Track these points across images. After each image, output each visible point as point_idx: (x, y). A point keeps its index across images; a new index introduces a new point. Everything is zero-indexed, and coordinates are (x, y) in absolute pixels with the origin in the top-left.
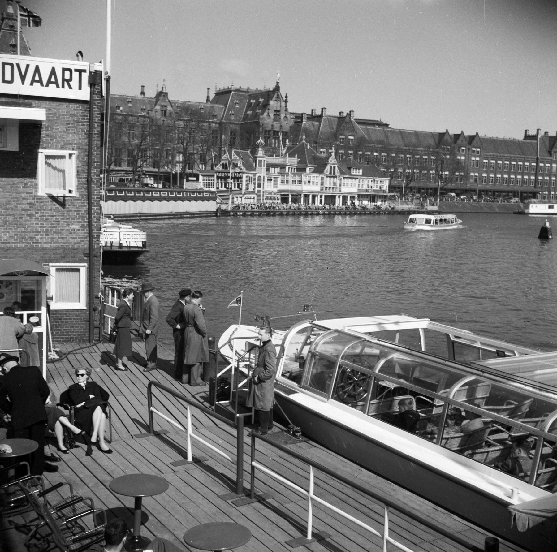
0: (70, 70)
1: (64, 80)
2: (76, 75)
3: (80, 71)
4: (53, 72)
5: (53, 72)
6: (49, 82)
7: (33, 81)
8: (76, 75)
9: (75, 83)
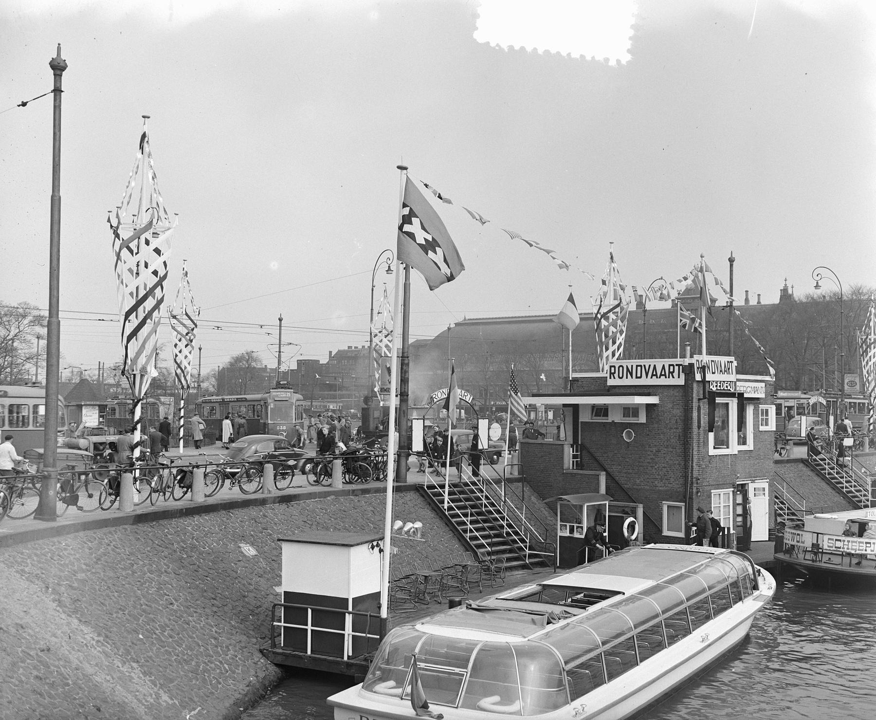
0: (673, 365)
1: (669, 372)
2: (676, 368)
3: (679, 365)
4: (664, 367)
5: (664, 367)
6: (661, 375)
7: (653, 375)
8: (676, 368)
9: (676, 374)
